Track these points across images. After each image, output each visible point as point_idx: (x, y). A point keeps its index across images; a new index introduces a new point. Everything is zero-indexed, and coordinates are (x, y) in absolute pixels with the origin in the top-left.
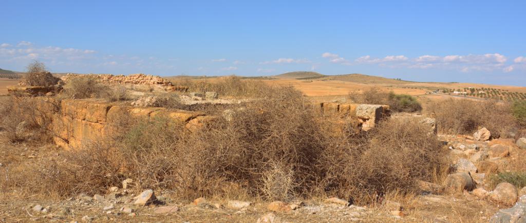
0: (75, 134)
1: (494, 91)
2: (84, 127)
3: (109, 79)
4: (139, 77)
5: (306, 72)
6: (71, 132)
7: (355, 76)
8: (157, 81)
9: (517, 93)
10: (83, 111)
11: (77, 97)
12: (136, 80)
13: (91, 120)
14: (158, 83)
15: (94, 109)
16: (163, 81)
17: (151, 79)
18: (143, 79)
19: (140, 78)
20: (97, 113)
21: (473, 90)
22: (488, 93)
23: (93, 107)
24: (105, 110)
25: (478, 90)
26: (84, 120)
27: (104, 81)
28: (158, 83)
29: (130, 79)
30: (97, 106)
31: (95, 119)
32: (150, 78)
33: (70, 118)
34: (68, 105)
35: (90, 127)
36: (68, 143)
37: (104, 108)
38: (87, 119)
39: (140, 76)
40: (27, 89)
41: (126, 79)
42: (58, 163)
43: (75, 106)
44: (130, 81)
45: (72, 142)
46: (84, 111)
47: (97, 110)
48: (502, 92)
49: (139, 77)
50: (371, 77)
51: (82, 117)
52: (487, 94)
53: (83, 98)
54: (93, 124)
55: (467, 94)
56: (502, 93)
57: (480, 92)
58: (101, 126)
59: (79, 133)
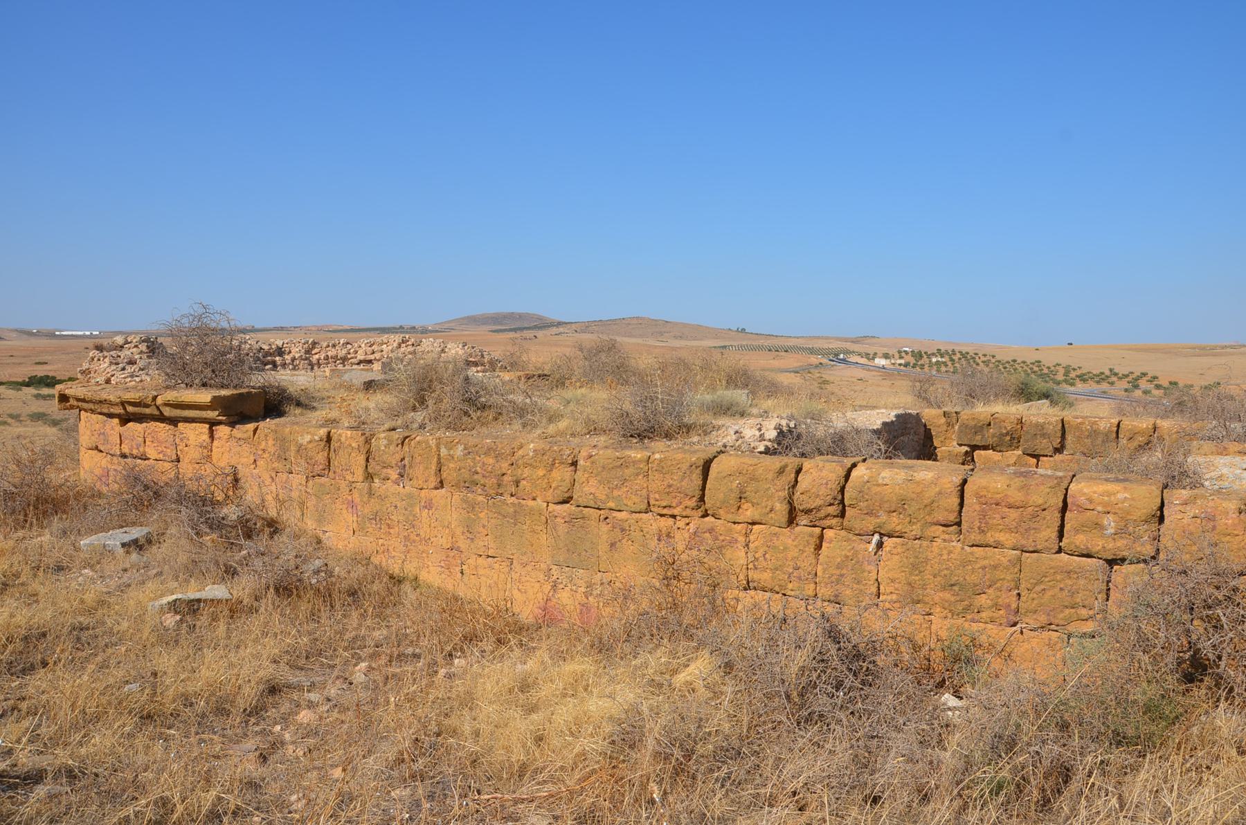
1: (964, 355)
3: (308, 352)
4: (399, 346)
7: (635, 321)
9: (1014, 361)
13: (611, 505)
21: (918, 355)
22: (952, 360)
24: (699, 471)
25: (929, 356)
27: (293, 359)
42: (1222, 664)
44: (372, 357)
48: (983, 359)
49: (399, 346)
50: (676, 324)
52: (949, 363)
55: (906, 365)
57: (934, 360)
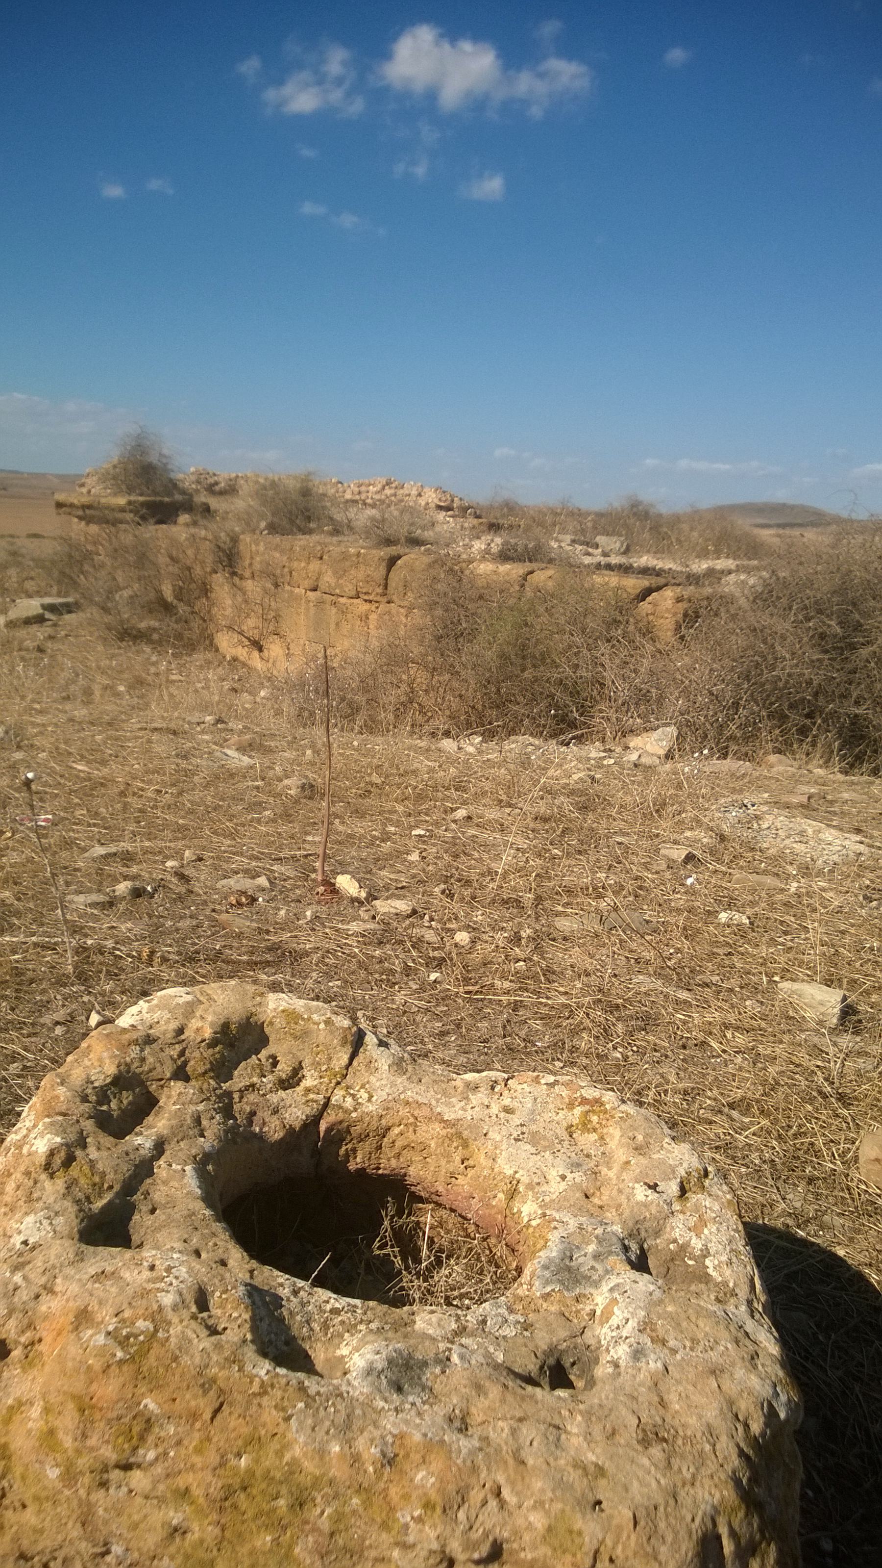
0: (284, 627)
2: (312, 611)
4: (383, 488)
5: (784, 505)
6: (274, 625)
8: (436, 501)
10: (311, 567)
11: (273, 528)
12: (377, 497)
13: (337, 591)
14: (440, 508)
15: (348, 563)
16: (453, 501)
17: (420, 495)
18: (395, 495)
19: (388, 491)
20: (360, 574)
23: (345, 556)
24: (384, 564)
26: (315, 590)
28: (440, 508)
29: (359, 493)
30: (358, 555)
31: (349, 589)
32: (414, 492)
33: (269, 585)
34: (261, 548)
35: (334, 610)
36: (261, 650)
37: (381, 559)
38: (323, 586)
39: (387, 484)
40: (130, 503)
41: (349, 491)
43: (282, 552)
44: (357, 497)
45: (275, 649)
46: (315, 566)
47: (356, 566)
49: (383, 488)
51: (307, 583)
53: (291, 533)
54: (343, 600)
56: (727, 747)
58: (367, 606)
59: (299, 624)
